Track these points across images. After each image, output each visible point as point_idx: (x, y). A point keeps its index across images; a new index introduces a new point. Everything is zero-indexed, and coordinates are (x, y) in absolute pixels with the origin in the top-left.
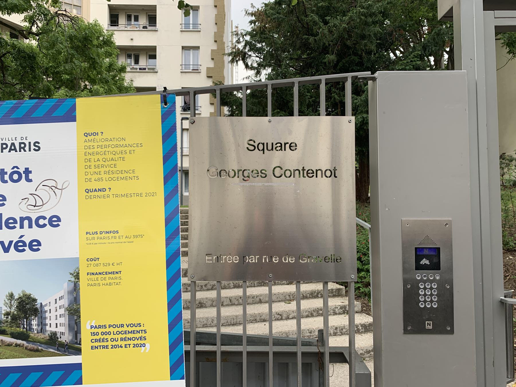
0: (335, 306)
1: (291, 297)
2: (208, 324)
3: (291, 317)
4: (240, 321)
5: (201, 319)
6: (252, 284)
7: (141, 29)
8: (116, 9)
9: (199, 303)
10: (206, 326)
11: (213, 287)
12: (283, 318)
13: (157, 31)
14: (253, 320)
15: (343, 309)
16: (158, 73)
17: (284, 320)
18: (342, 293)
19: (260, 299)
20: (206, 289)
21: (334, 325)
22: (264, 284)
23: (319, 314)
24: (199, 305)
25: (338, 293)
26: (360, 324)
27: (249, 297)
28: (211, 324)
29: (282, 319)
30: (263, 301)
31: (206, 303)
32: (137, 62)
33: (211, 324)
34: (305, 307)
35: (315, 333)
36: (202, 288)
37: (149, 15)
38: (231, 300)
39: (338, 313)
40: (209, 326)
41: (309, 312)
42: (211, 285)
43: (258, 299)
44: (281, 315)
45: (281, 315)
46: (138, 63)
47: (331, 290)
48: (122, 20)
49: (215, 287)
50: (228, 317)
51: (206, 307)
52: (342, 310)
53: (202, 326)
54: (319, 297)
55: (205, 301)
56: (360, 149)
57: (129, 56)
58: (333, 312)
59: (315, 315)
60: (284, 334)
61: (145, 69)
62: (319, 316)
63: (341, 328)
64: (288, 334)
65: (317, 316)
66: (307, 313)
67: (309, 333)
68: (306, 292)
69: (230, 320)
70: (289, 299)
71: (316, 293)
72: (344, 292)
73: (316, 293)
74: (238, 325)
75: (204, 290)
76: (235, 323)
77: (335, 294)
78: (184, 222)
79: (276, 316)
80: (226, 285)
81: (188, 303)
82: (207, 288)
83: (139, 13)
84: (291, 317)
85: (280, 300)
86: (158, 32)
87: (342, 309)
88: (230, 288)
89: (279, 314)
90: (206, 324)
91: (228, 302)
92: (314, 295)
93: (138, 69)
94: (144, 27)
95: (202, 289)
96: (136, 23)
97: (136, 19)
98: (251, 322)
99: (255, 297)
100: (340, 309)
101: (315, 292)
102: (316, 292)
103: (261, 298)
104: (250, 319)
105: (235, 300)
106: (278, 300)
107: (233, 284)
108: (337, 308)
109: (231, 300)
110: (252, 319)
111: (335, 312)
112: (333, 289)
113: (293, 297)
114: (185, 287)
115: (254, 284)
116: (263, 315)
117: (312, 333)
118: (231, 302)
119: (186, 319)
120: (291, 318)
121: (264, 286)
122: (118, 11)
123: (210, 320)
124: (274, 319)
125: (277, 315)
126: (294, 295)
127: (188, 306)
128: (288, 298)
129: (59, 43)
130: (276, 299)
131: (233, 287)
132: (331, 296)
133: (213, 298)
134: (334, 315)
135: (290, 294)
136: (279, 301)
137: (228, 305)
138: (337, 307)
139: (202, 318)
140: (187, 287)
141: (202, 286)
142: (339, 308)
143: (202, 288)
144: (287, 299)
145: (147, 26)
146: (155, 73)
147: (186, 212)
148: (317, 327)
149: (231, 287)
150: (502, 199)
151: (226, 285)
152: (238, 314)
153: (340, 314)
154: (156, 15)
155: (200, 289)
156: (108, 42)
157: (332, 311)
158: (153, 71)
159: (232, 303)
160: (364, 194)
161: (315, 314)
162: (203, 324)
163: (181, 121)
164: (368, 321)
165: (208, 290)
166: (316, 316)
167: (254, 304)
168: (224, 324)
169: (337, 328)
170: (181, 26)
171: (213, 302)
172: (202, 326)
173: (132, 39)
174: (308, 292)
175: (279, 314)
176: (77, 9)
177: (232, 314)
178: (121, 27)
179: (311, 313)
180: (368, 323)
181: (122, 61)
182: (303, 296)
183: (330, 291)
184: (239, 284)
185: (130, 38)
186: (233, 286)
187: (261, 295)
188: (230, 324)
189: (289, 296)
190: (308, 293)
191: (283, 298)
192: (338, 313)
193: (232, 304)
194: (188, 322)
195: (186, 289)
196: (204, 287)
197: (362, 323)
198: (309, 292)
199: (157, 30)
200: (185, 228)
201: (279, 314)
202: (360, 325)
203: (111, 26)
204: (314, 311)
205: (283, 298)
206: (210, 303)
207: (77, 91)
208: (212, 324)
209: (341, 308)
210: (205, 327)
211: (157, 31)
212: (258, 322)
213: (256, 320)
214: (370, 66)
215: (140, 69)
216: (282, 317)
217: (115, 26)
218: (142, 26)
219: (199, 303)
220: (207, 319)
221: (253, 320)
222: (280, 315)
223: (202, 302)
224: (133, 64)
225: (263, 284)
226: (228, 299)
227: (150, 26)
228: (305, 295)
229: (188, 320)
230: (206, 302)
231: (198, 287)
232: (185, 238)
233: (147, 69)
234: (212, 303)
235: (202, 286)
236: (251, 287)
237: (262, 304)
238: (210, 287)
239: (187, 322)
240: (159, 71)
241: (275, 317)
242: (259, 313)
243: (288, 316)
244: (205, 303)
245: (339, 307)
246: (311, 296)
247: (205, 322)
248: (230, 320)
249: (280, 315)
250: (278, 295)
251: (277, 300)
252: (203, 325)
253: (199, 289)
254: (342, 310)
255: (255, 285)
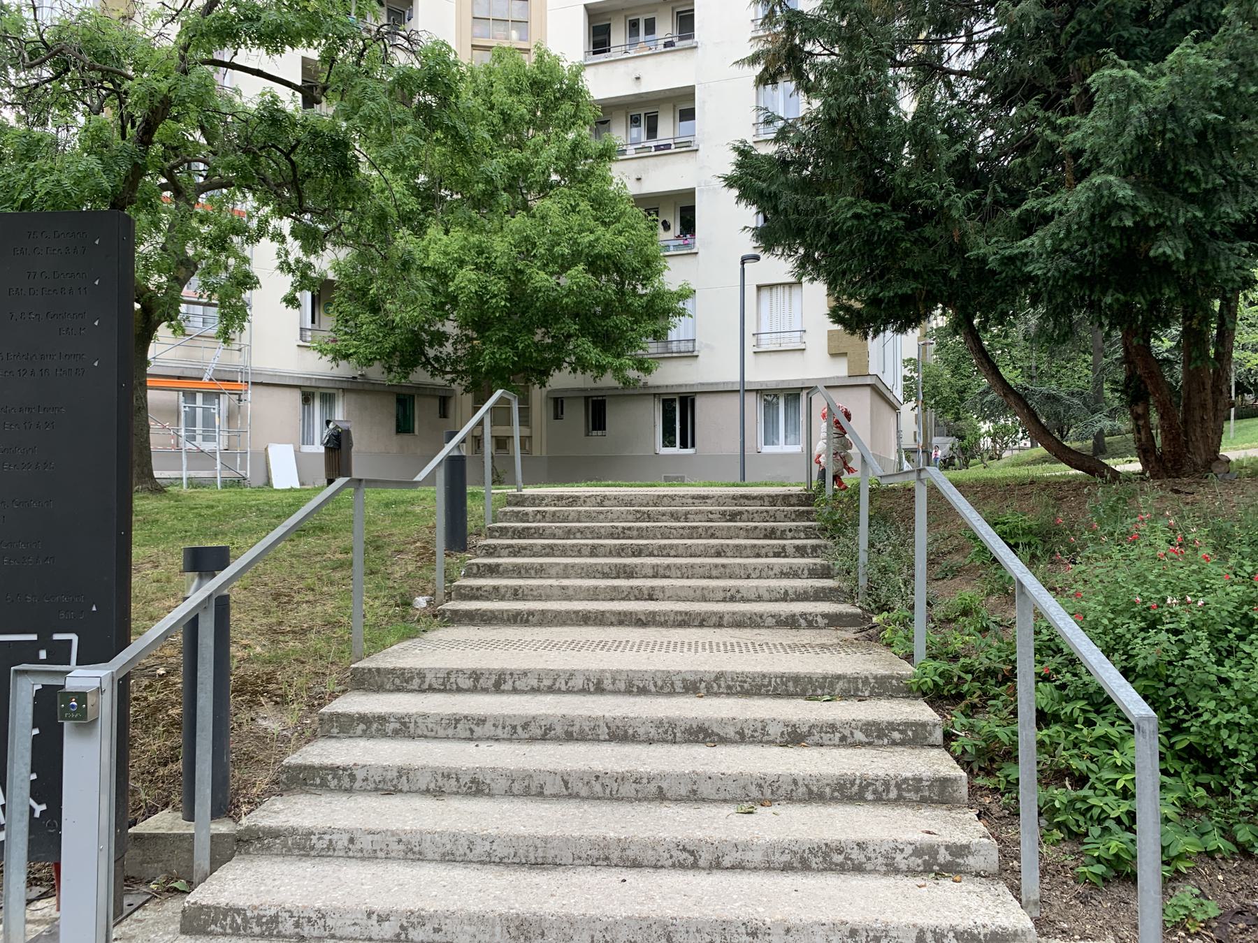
0: (892, 845)
1: (768, 792)
2: (458, 853)
3: (727, 862)
4: (556, 856)
5: (436, 836)
6: (666, 732)
7: (661, 48)
8: (603, 13)
9: (472, 782)
10: (451, 857)
11: (546, 734)
12: (701, 863)
13: (696, 47)
14: (598, 859)
15: (927, 858)
16: (699, 153)
17: (704, 869)
18: (956, 795)
19: (659, 787)
20: (527, 736)
21: (844, 919)
22: (704, 738)
23: (832, 863)
24: (470, 788)
25: (942, 792)
26: (953, 928)
27: (623, 780)
28: (465, 854)
29: (695, 866)
30: (668, 795)
31: (493, 785)
32: (652, 132)
33: (465, 854)
34: (782, 836)
35: (770, 938)
36: (515, 732)
37: (678, 13)
38: (566, 783)
39: (905, 868)
40: (460, 859)
41: (795, 853)
42: (541, 727)
43: (652, 788)
44: (692, 853)
45: (692, 853)
46: (655, 137)
47: (914, 779)
48: (618, 37)
49: (553, 732)
50: (518, 838)
51: (491, 795)
52: (920, 861)
53: (438, 858)
54: (866, 801)
55: (487, 777)
56: (1122, 297)
57: (635, 121)
58: (886, 865)
59: (814, 866)
60: (654, 927)
61: (668, 146)
62: (832, 870)
63: (871, 934)
64: (671, 928)
65: (825, 869)
66: (786, 858)
67: (748, 934)
68: (818, 781)
69: (525, 848)
70: (760, 796)
71: (856, 787)
72: (964, 791)
73: (856, 787)
74: (548, 869)
75: (520, 740)
76: (540, 860)
77: (927, 794)
78: (623, 528)
79: (675, 853)
80: (587, 729)
81: (440, 779)
82: (531, 733)
83: (656, 11)
84: (727, 862)
85: (728, 797)
86: (699, 50)
87: (920, 857)
88: (599, 740)
89: (684, 849)
90: (453, 854)
91: (559, 788)
92: (848, 793)
93: (653, 149)
94: (666, 45)
95: (515, 736)
96: (650, 37)
97: (650, 27)
98: (592, 865)
99: (645, 781)
100: (911, 855)
101: (853, 783)
102: (858, 782)
103: (665, 785)
104: (589, 852)
105: (581, 785)
106: (722, 795)
107: (606, 730)
108: (902, 851)
109: (566, 783)
110: (594, 853)
111: (891, 865)
112: (921, 780)
113: (772, 793)
114: (467, 727)
115: (675, 734)
116: (632, 847)
117: (760, 936)
118: (567, 788)
119: (392, 831)
120: (729, 865)
121: (705, 743)
122: (609, 17)
123: (463, 841)
124: (670, 862)
125: (679, 853)
126: (776, 785)
127: (440, 788)
128: (755, 793)
129: (369, 100)
130: (713, 792)
131: (607, 737)
132: (911, 801)
133: (511, 771)
134: (886, 874)
135: (760, 781)
136: (725, 801)
137: (556, 796)
138: (901, 847)
139: (441, 834)
140: (472, 726)
141: (514, 727)
142: (911, 852)
143: (515, 732)
144: (752, 796)
145: (675, 40)
146: (693, 154)
147: (645, 502)
148: (779, 917)
149: (602, 737)
150: (995, 560)
151: (587, 729)
152: (550, 833)
153: (911, 872)
154: (693, 10)
155: (509, 736)
156: (573, 93)
157: (881, 860)
158: (688, 148)
159: (570, 791)
160: (1199, 449)
161: (814, 861)
162: (442, 850)
163: (740, 266)
164: (989, 923)
165: (532, 739)
166: (819, 871)
167: (640, 800)
168: (506, 860)
169: (857, 931)
170: (753, 25)
171: (513, 781)
172: (438, 858)
173: (638, 78)
174: (825, 782)
175: (687, 847)
176: (518, 29)
177: (532, 831)
178: (615, 53)
179: (802, 857)
180: (986, 931)
181: (619, 134)
182: (810, 792)
183: (909, 785)
184: (626, 732)
185: (634, 76)
186: (608, 734)
187: (663, 776)
188: (524, 861)
189: (760, 786)
190: (828, 785)
191: (739, 792)
192: (903, 867)
193: (570, 794)
194: (400, 841)
195: (469, 732)
196: (519, 730)
197: (960, 928)
198: (828, 782)
199: (694, 45)
200: (615, 545)
201: (684, 849)
202: (951, 935)
203: (595, 53)
204: (811, 852)
205: (739, 792)
206: (503, 784)
207: (1169, 256)
208: (470, 856)
209: (918, 852)
210: (448, 861)
211: (696, 47)
212: (616, 866)
213: (607, 858)
214: (1188, 19)
215: (657, 148)
216: (696, 861)
217: (604, 51)
218: (663, 42)
219: (472, 782)
220: (455, 837)
221: (598, 859)
222: (689, 851)
223: (481, 778)
224: (643, 137)
225: (701, 736)
226: (558, 778)
227: (681, 39)
228: (815, 789)
229: (398, 834)
230: (493, 780)
231: (504, 728)
232: (604, 573)
233: (673, 146)
234: (510, 787)
235: (514, 727)
236: (665, 741)
237: (666, 803)
238: (539, 732)
239: (395, 839)
240: (701, 148)
241: (671, 857)
242: (620, 840)
243: (718, 857)
244: (488, 781)
245: (909, 850)
246: (836, 794)
247: (448, 847)
248: (525, 848)
249: (689, 851)
250: (719, 781)
251: (717, 797)
252: (444, 855)
253: (505, 736)
254: (920, 861)
255: (677, 739)
